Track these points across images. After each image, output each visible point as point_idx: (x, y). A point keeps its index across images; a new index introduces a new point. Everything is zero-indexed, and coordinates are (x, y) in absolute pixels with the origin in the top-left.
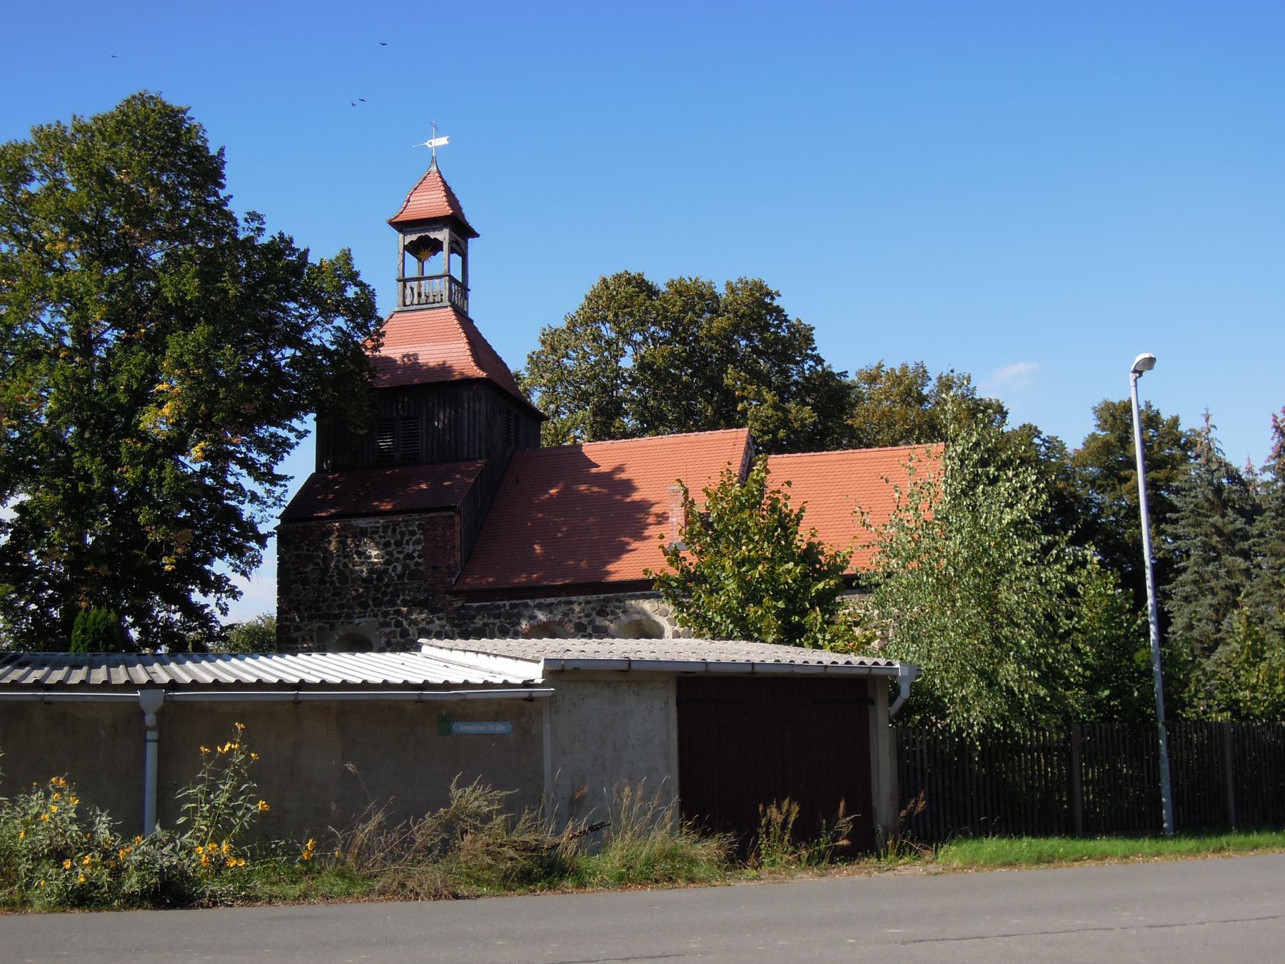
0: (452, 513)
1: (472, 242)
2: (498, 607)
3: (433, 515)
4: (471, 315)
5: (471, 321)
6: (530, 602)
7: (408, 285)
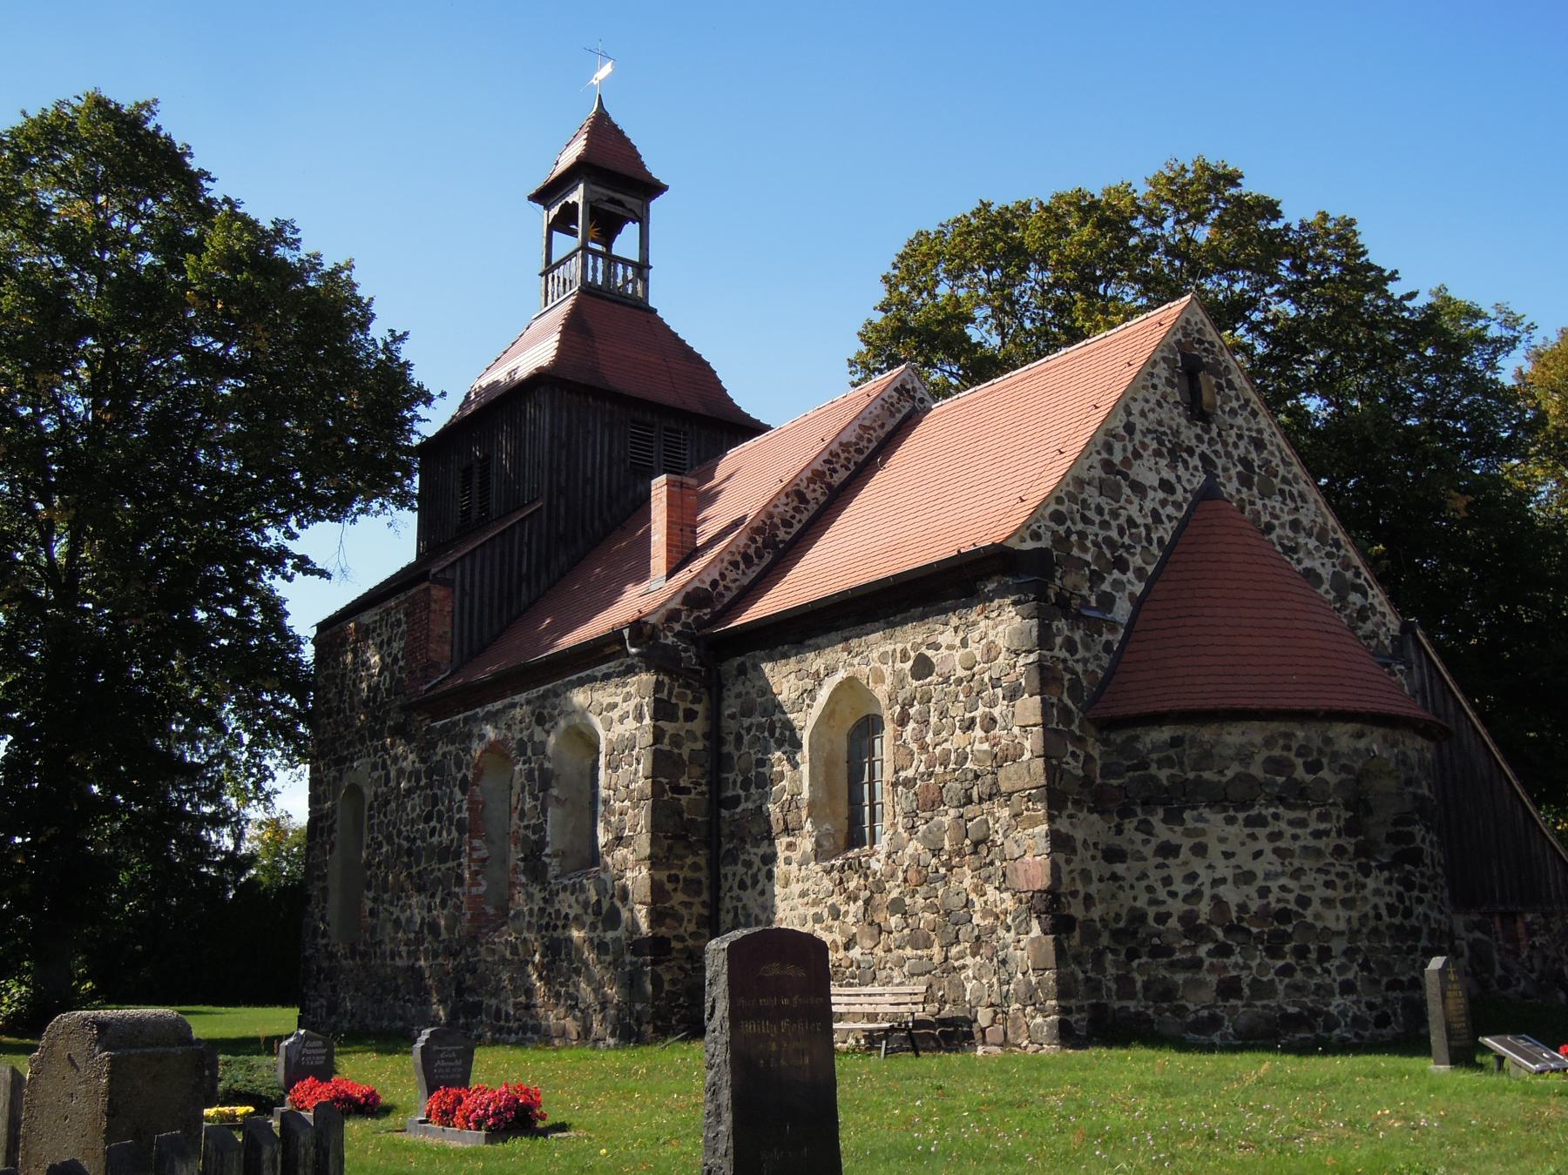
0: (427, 584)
1: (656, 206)
2: (455, 724)
3: (414, 591)
4: (651, 304)
5: (654, 311)
6: (480, 711)
7: (550, 276)
